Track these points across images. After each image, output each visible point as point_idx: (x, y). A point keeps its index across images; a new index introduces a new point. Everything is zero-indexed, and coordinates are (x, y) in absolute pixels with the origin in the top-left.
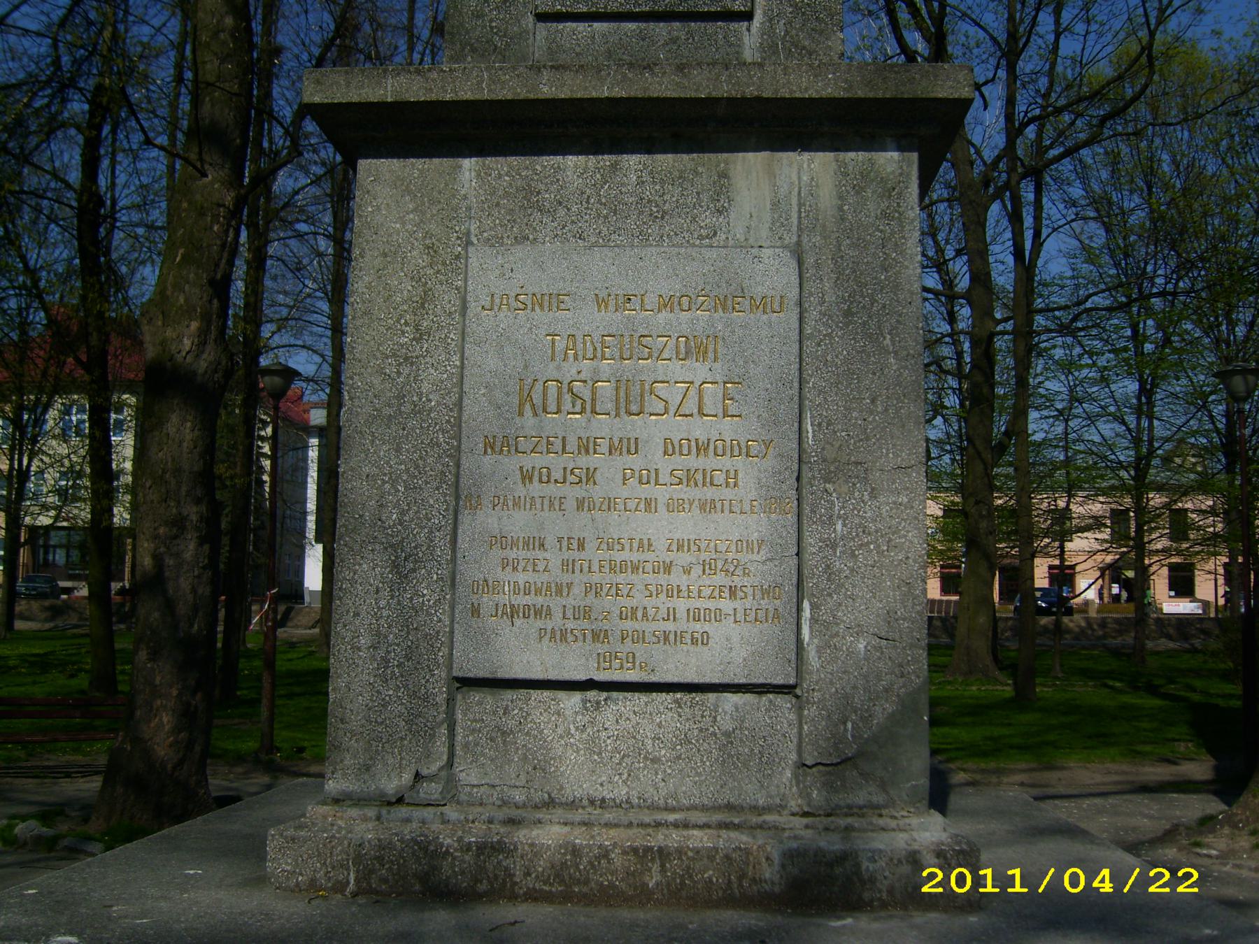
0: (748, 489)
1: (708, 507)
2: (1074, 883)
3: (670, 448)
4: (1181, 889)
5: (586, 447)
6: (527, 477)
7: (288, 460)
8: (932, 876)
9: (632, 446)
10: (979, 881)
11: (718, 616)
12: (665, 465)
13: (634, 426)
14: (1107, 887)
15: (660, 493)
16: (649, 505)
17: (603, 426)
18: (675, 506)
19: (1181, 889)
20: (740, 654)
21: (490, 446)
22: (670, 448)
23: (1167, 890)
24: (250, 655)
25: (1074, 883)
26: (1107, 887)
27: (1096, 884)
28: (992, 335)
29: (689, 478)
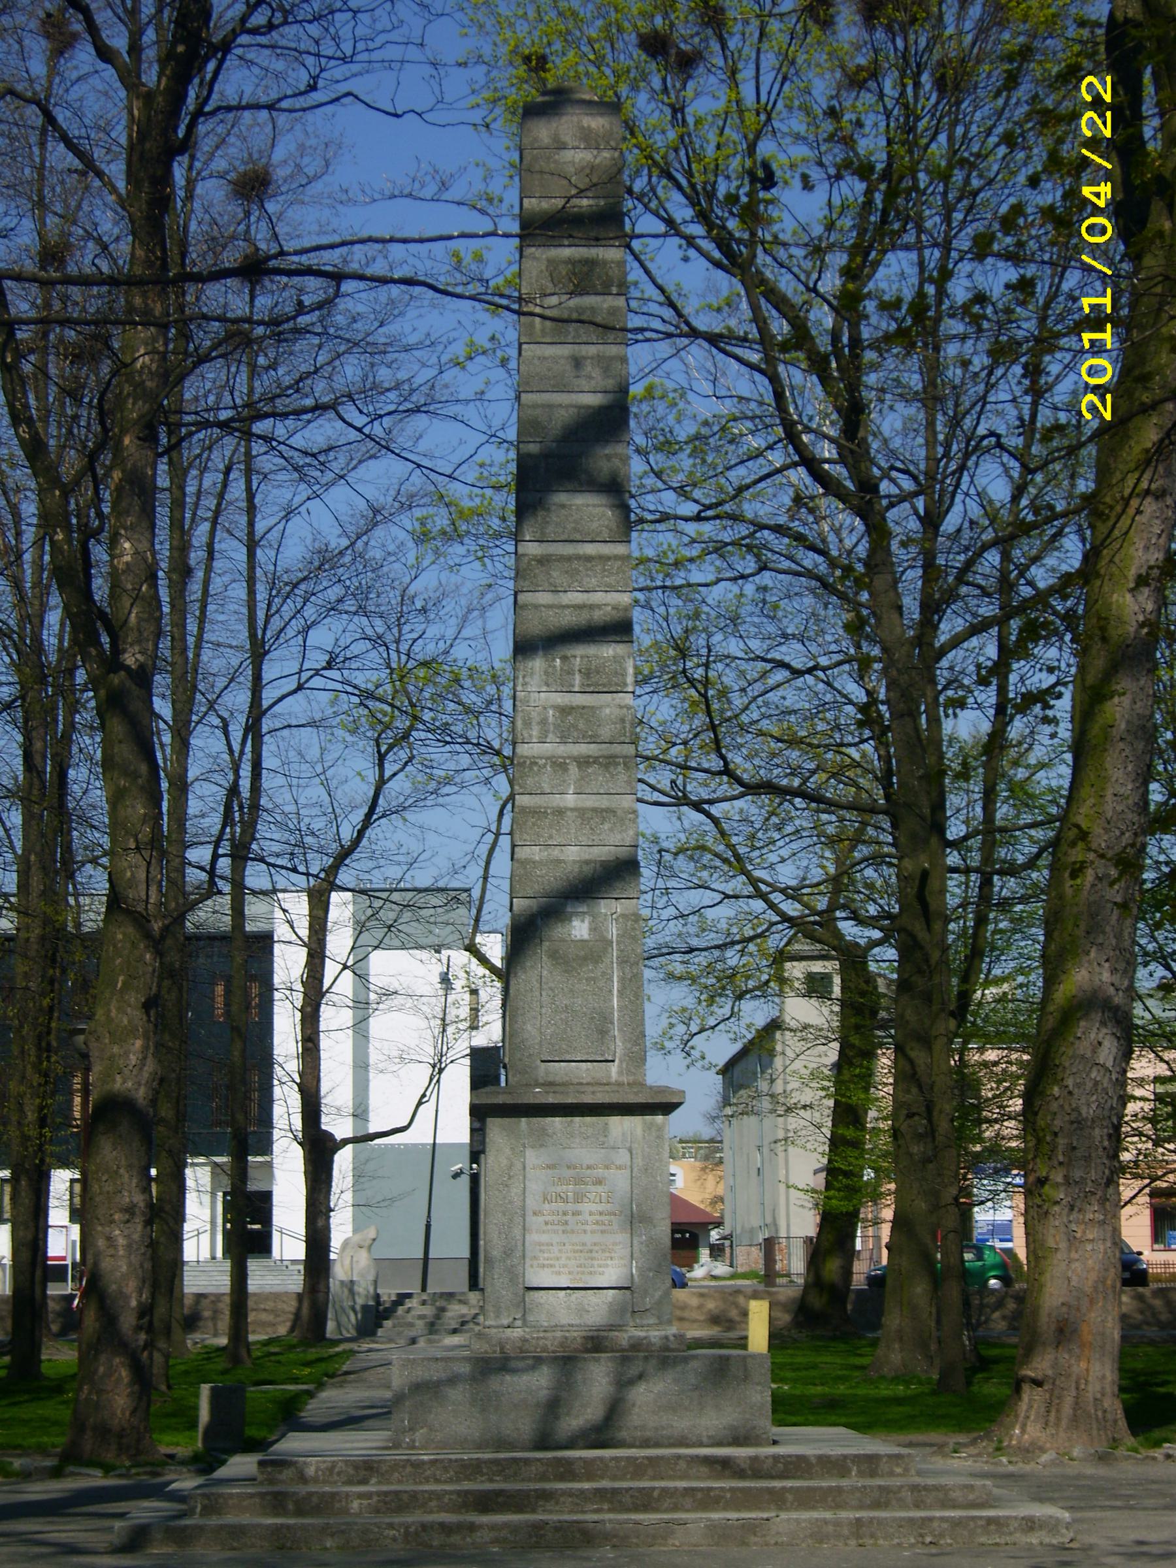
0: (615, 1227)
1: (603, 1232)
2: (1091, 229)
3: (591, 1214)
4: (1108, 98)
5: (565, 1214)
6: (546, 1223)
7: (688, 1502)
8: (1092, 408)
9: (576, 1213)
10: (1096, 321)
11: (607, 1266)
12: (590, 1219)
13: (579, 1207)
14: (1106, 189)
15: (588, 1228)
16: (585, 1232)
17: (570, 1207)
18: (593, 1232)
19: (1108, 98)
20: (614, 1278)
21: (535, 1214)
22: (591, 1214)
23: (1109, 114)
24: (59, 1273)
25: (1091, 229)
26: (1106, 189)
27: (1101, 203)
28: (110, 336)
29: (597, 1223)
